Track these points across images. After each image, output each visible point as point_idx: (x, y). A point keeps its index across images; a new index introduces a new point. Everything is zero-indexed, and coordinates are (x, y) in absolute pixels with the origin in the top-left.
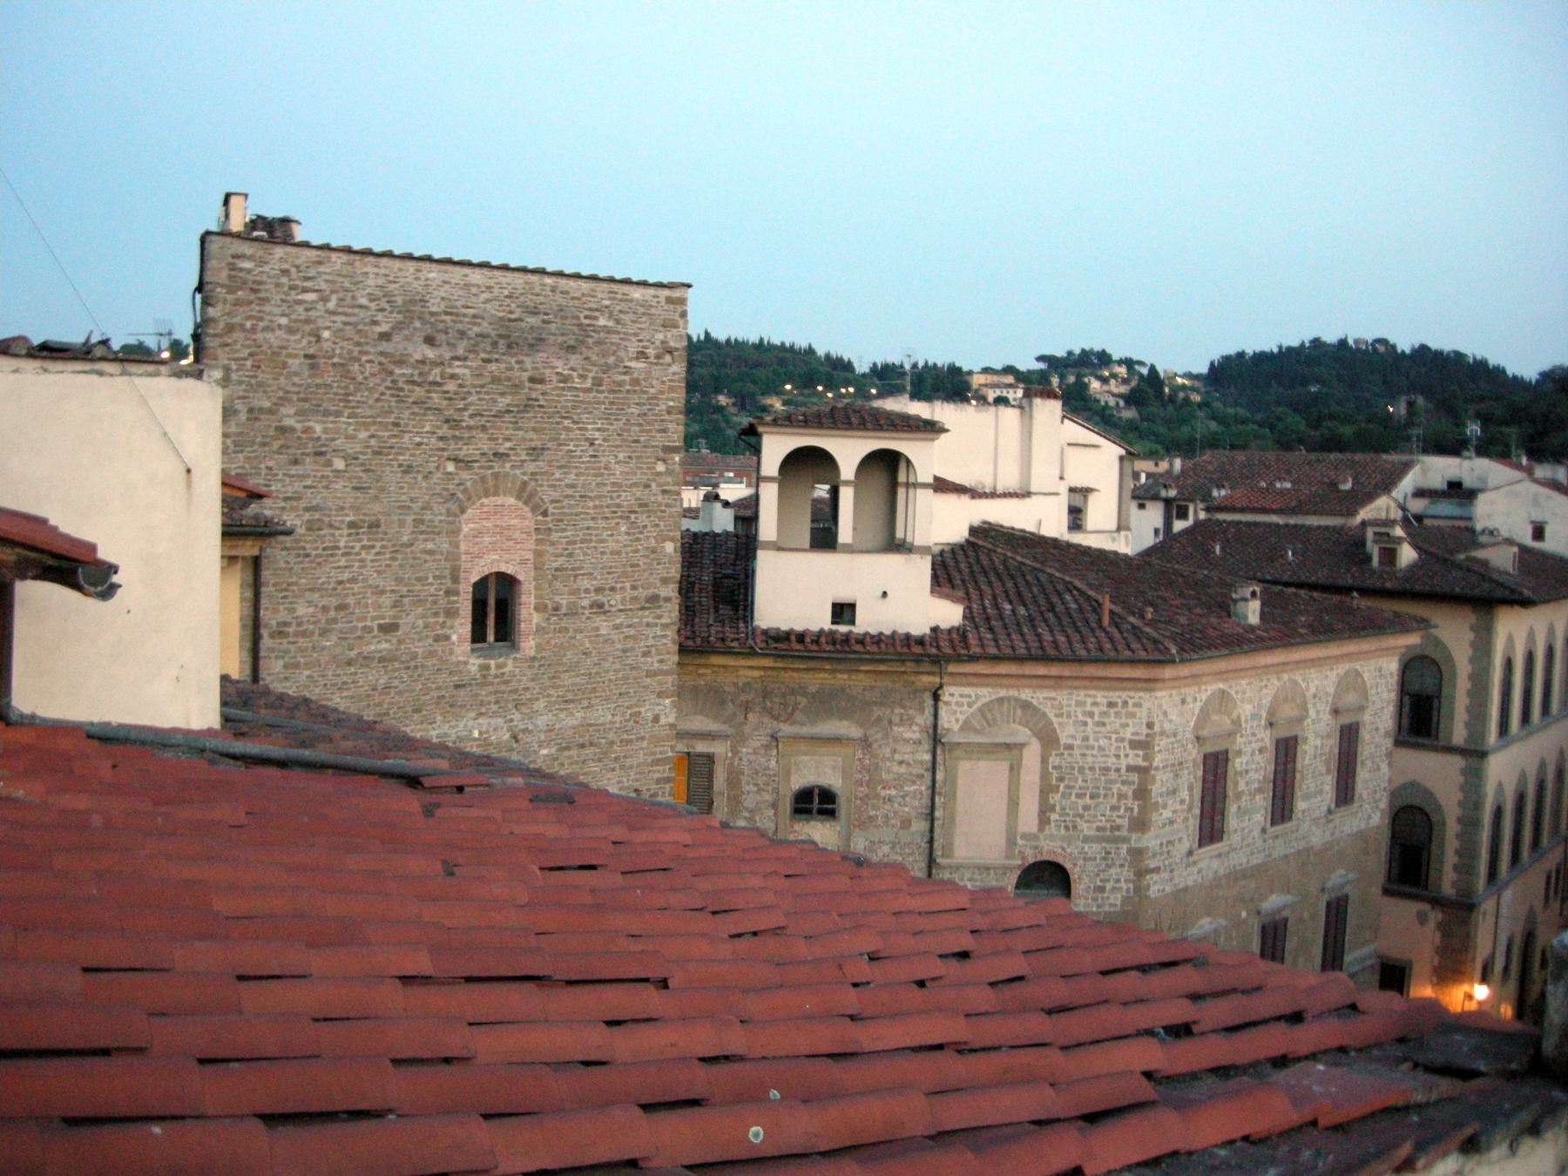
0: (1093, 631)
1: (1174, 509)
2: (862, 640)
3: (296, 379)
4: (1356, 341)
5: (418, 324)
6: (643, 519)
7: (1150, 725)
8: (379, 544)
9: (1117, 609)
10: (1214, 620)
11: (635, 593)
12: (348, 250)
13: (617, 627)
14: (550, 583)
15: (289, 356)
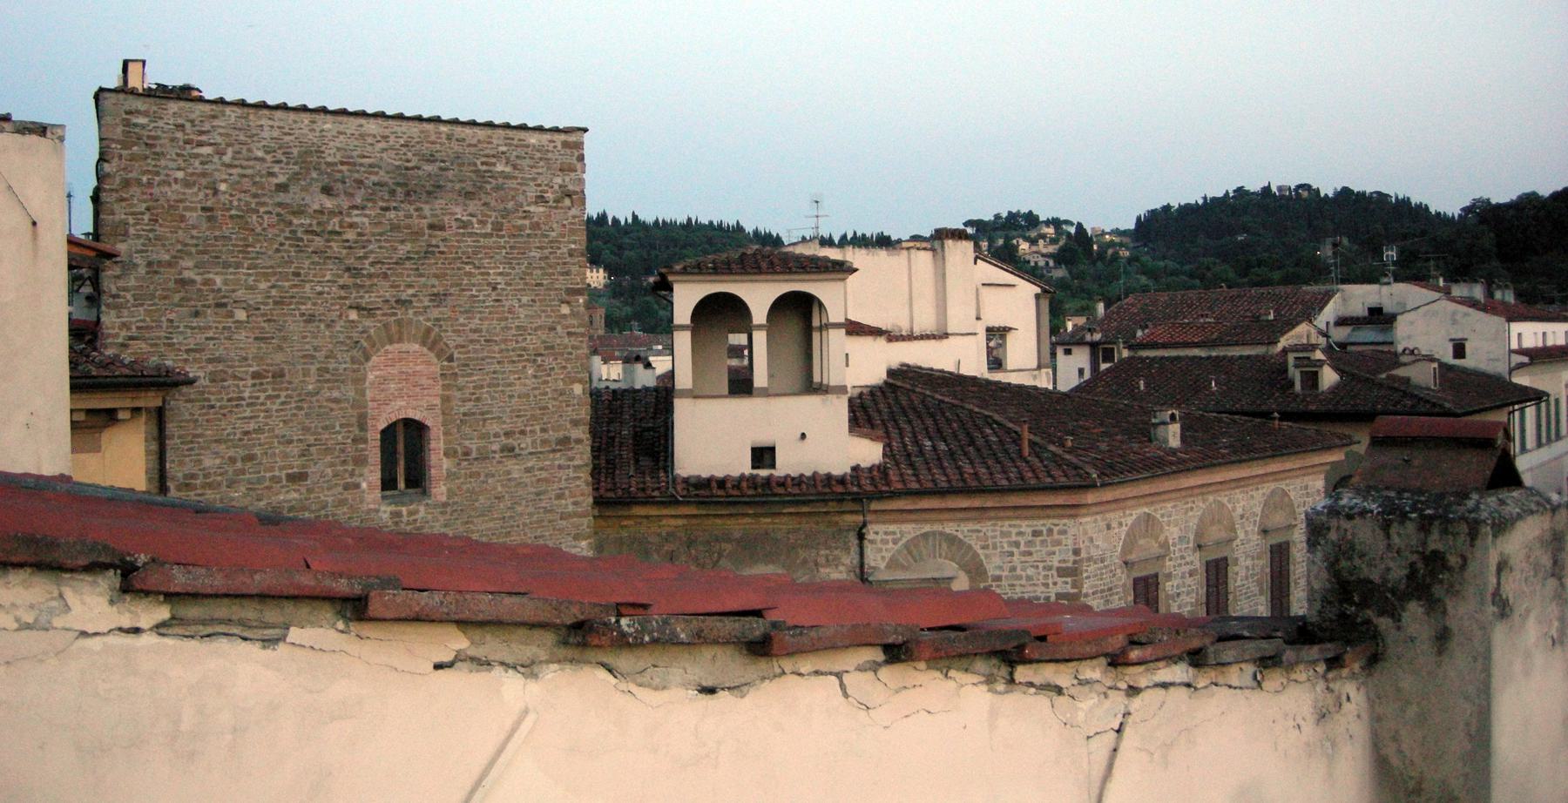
0: (1013, 460)
1: (1099, 351)
2: (783, 482)
3: (194, 232)
4: (1280, 188)
5: (314, 175)
6: (549, 361)
7: (1076, 552)
8: (283, 394)
9: (1037, 439)
10: (1136, 446)
11: (546, 436)
12: (242, 104)
13: (528, 470)
14: (459, 428)
15: (186, 209)
